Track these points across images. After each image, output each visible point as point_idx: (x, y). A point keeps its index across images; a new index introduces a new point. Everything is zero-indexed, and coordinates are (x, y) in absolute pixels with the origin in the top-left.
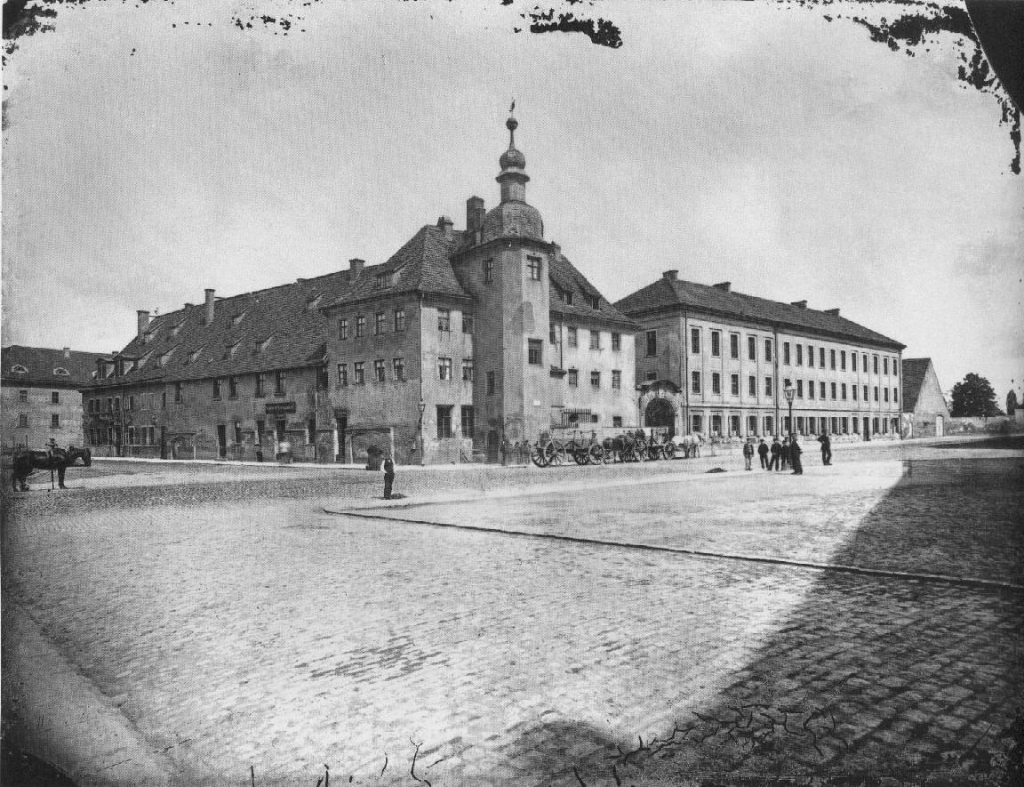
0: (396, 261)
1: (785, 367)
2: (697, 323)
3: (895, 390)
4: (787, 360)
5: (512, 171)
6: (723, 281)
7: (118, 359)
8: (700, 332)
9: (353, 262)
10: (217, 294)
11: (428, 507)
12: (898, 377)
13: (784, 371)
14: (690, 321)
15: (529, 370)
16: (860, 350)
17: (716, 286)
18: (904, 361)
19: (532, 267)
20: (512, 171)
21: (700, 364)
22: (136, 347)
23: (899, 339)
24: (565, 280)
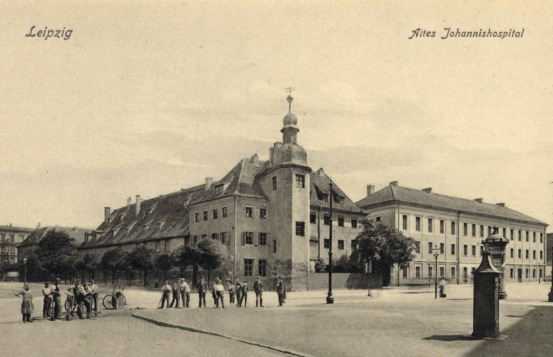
0: (225, 179)
1: (299, 238)
2: (406, 212)
3: (541, 252)
4: (466, 233)
5: (289, 131)
6: (428, 187)
7: (94, 233)
8: (408, 217)
9: (207, 179)
10: (141, 198)
11: (164, 328)
12: (542, 244)
13: (464, 240)
14: (401, 211)
15: (295, 238)
16: (531, 229)
17: (424, 190)
18: (549, 235)
19: (299, 181)
20: (289, 131)
21: (317, 235)
22: (103, 226)
23: (544, 221)
24: (324, 188)
